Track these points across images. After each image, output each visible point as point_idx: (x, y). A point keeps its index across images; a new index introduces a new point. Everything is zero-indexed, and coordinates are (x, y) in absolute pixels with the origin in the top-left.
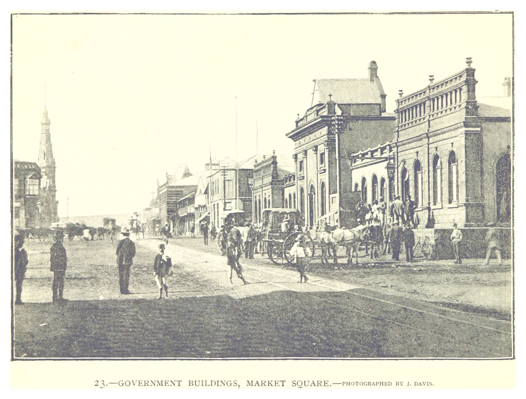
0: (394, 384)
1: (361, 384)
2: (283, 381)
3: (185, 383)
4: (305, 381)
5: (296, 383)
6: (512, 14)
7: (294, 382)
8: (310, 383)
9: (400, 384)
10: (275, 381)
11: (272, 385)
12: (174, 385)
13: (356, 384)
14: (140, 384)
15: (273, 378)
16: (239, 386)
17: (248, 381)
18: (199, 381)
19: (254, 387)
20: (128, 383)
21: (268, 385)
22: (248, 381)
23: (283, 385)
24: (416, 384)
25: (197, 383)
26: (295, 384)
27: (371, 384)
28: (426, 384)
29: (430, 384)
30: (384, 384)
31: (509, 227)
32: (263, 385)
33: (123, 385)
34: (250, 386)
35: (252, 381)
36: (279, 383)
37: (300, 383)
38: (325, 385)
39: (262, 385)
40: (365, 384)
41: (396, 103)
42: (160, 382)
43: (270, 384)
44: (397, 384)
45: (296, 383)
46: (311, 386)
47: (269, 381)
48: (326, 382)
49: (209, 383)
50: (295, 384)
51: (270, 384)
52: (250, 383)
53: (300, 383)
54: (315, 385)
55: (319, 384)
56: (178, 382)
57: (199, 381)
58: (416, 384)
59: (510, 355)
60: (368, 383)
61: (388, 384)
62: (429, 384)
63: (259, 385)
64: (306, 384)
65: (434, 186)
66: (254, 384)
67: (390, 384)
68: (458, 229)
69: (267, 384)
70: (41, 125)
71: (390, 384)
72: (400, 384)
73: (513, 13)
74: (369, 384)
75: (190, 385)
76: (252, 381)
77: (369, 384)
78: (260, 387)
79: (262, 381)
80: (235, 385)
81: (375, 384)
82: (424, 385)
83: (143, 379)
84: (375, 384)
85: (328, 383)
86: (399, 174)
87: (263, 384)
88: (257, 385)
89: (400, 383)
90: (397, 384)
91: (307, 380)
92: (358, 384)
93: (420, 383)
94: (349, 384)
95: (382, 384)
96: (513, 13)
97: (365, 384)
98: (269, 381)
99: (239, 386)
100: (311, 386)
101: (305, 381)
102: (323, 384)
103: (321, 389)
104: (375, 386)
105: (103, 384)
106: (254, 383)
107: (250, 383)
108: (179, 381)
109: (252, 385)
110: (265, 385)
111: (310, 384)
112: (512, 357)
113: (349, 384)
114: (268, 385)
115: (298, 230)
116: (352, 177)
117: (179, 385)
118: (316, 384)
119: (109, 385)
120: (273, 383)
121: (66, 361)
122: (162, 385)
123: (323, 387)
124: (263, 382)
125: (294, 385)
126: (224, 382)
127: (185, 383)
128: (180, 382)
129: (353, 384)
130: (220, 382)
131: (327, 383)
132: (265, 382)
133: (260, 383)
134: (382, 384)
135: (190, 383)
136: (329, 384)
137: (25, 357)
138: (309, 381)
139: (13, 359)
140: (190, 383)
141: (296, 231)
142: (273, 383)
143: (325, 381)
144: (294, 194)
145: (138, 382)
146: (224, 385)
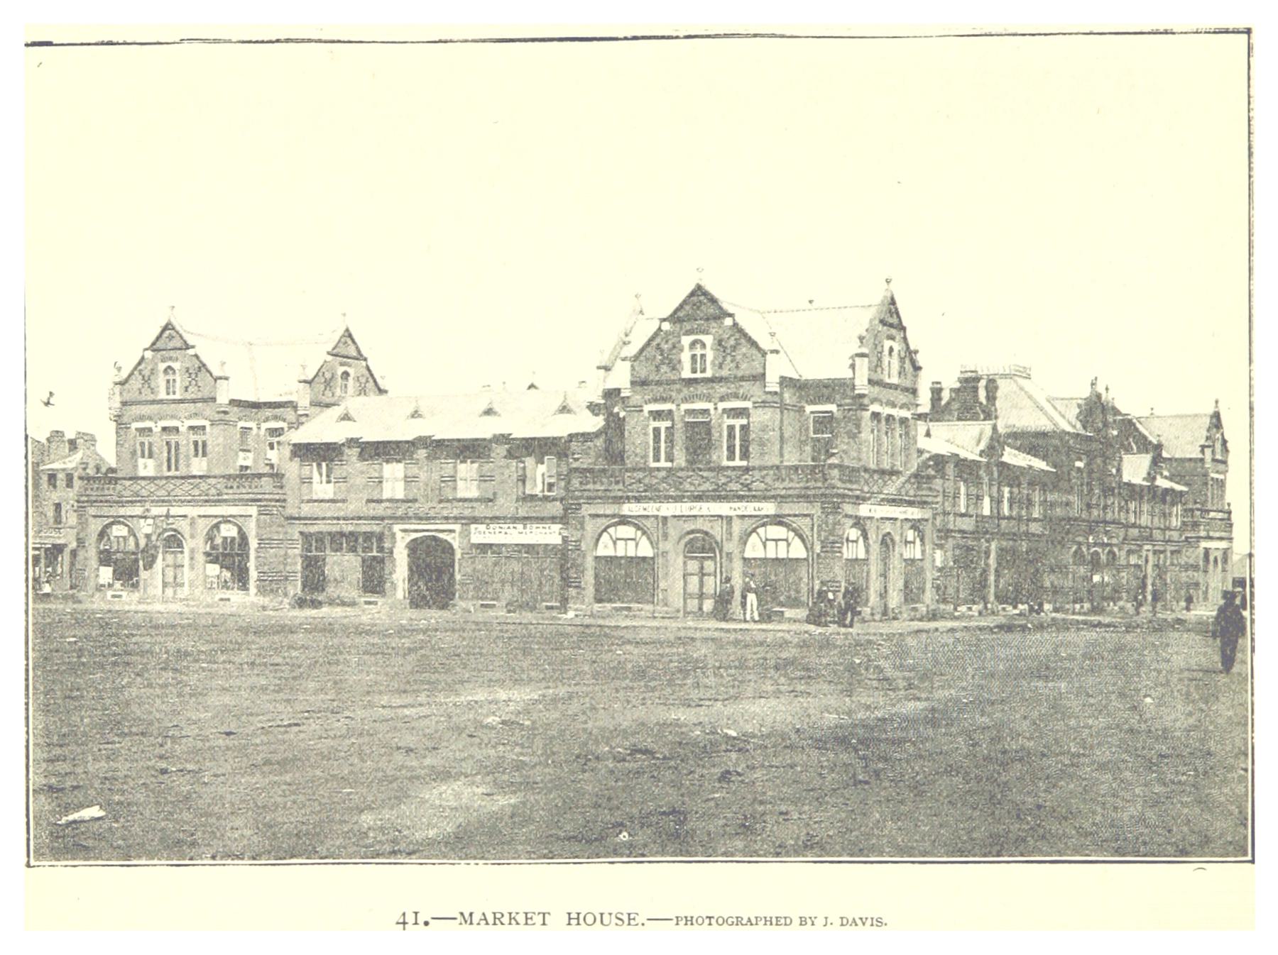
0: (796, 921)
1: (720, 921)
2: (544, 914)
3: (557, 919)
4: (602, 914)
6: (1246, 36)
9: (809, 922)
10: (526, 914)
11: (518, 924)
13: (707, 921)
15: (519, 906)
18: (610, 914)
19: (475, 926)
20: (590, 919)
23: (544, 924)
24: (844, 922)
27: (744, 922)
28: (869, 922)
29: (879, 922)
30: (774, 921)
31: (316, 549)
32: (497, 922)
34: (467, 926)
35: (471, 914)
36: (535, 917)
40: (730, 922)
42: (467, 916)
43: (513, 921)
44: (803, 922)
47: (510, 914)
51: (513, 921)
57: (610, 914)
58: (844, 922)
59: (1245, 854)
60: (735, 920)
62: (875, 922)
63: (487, 924)
65: (440, 444)
66: (475, 920)
69: (506, 920)
72: (809, 922)
73: (1248, 31)
75: (569, 924)
76: (471, 914)
78: (491, 927)
79: (494, 914)
81: (754, 921)
82: (864, 924)
83: (520, 907)
85: (637, 917)
87: (497, 919)
91: (869, 917)
92: (713, 921)
93: (749, 920)
94: (689, 921)
95: (768, 921)
96: (1248, 31)
97: (730, 922)
98: (510, 914)
101: (602, 914)
106: (476, 919)
109: (471, 923)
112: (1249, 858)
113: (689, 921)
118: (490, 919)
119: (432, 922)
133: (490, 919)
134: (768, 921)
135: (570, 919)
136: (639, 920)
139: (1253, 862)
140: (574, 919)
142: (521, 918)
144: (196, 455)
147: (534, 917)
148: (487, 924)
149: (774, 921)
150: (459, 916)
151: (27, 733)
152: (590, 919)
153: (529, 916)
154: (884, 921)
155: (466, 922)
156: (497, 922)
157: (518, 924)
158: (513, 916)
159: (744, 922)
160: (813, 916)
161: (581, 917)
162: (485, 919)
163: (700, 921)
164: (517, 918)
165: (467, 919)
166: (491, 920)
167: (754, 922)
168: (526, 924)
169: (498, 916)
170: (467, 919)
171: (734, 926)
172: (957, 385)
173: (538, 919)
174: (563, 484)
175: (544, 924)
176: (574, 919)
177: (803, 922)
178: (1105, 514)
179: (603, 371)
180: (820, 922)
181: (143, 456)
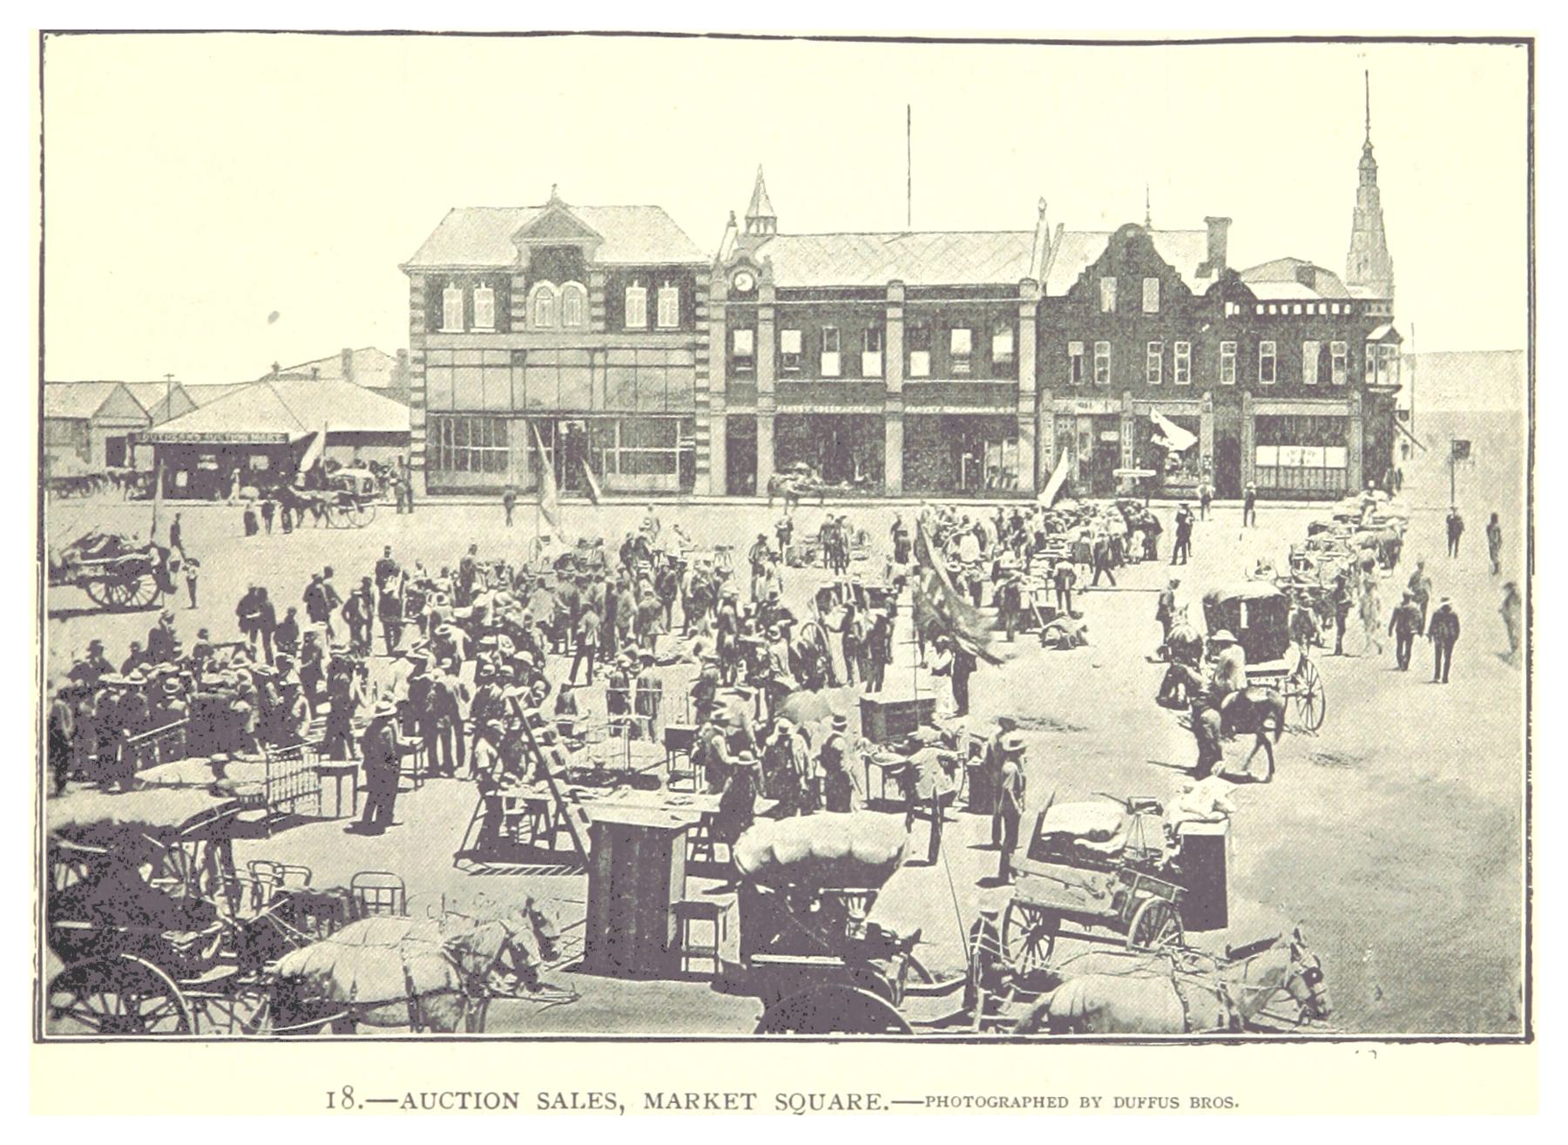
0: (1075, 1102)
1: (981, 1102)
2: (748, 1096)
4: (812, 1096)
5: (787, 1100)
7: (781, 1098)
8: (828, 1100)
9: (1092, 1102)
10: (727, 1096)
11: (716, 1107)
12: (515, 1104)
13: (964, 1102)
16: (622, 1108)
17: (648, 1095)
18: (434, 1094)
19: (664, 1110)
20: (492, 1101)
22: (648, 1095)
23: (463, 1107)
24: (1195, 1103)
25: (1131, 1102)
26: (783, 1102)
27: (1009, 1103)
29: (1228, 1103)
30: (1046, 1102)
32: (853, 1105)
34: (655, 1110)
35: (660, 1095)
37: (797, 1102)
38: (869, 1108)
39: (688, 1107)
40: (992, 1103)
41: (405, 282)
42: (654, 1097)
43: (710, 1105)
45: (787, 1100)
46: (668, 1107)
47: (707, 1095)
49: (583, 1099)
50: (783, 1102)
51: (710, 1105)
52: (654, 1101)
53: (797, 1102)
55: (853, 1104)
56: (460, 1096)
57: (434, 1094)
58: (1195, 1103)
61: (1057, 1102)
63: (679, 1107)
64: (817, 1104)
66: (665, 1103)
67: (1063, 1102)
68: (937, 729)
69: (701, 1102)
70: (408, 306)
71: (1063, 1102)
72: (1092, 1102)
74: (1003, 1102)
76: (660, 1095)
77: (1003, 1102)
78: (846, 1111)
79: (688, 1095)
80: (611, 1105)
81: (1021, 1102)
84: (1021, 1102)
87: (691, 1102)
88: (675, 1105)
89: (1091, 1102)
90: (1084, 1102)
91: (817, 1092)
92: (972, 1102)
94: (943, 1102)
95: (1039, 1102)
97: (992, 1103)
98: (707, 1095)
99: (622, 1108)
100: (668, 1107)
101: (812, 1096)
102: (864, 1103)
103: (861, 1116)
104: (1022, 1109)
106: (665, 1100)
107: (654, 1101)
108: (748, 1096)
109: (660, 1107)
110: (696, 1107)
113: (943, 1102)
117: (748, 1107)
118: (683, 1101)
119: (367, 1105)
120: (720, 1101)
121: (1062, 1046)
122: (660, 1107)
125: (781, 1106)
127: (764, 1102)
128: (752, 1097)
129: (956, 1102)
131: (875, 1102)
132: (698, 1097)
134: (1039, 1102)
136: (881, 1102)
138: (822, 1096)
142: (720, 1101)
143: (869, 1096)
147: (737, 1099)
148: (679, 1107)
149: (1046, 1102)
152: (492, 1101)
153: (730, 1098)
154: (1234, 1102)
155: (653, 1105)
160: (1097, 1096)
161: (482, 1098)
162: (677, 1102)
163: (956, 1102)
164: (716, 1100)
168: (591, 1107)
169: (854, 1098)
171: (998, 1108)
172: (88, 653)
173: (741, 1102)
174: (248, 647)
177: (1084, 1102)
178: (407, 776)
180: (1185, 1102)
181: (613, 470)
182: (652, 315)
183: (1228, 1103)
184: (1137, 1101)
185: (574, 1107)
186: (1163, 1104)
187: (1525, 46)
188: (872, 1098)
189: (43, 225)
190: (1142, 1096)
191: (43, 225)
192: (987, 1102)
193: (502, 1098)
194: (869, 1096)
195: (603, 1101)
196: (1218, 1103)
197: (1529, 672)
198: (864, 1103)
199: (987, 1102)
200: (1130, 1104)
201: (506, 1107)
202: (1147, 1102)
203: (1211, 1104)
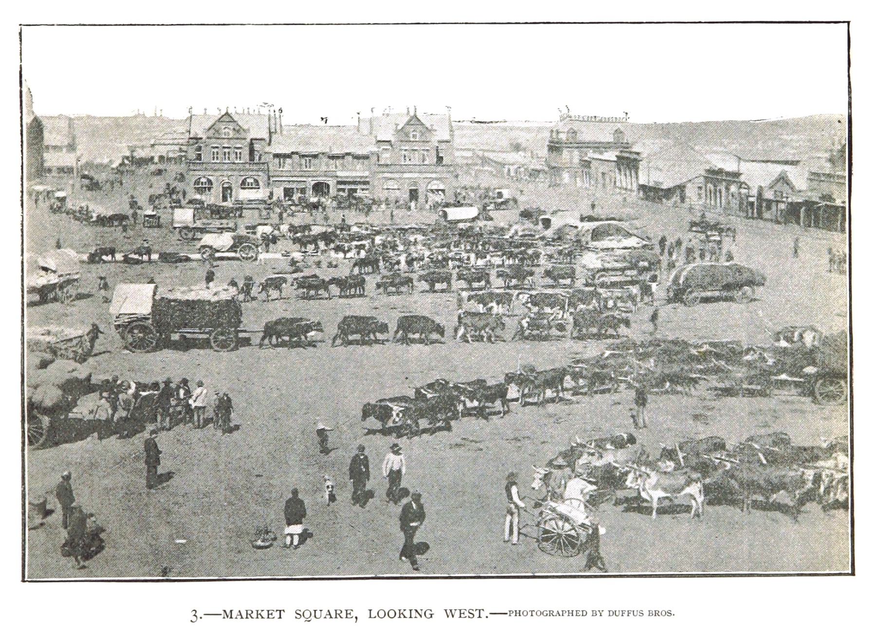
0: (590, 613)
1: (539, 613)
2: (280, 611)
3: (290, 615)
4: (315, 611)
5: (302, 614)
7: (298, 612)
8: (324, 613)
9: (598, 614)
10: (268, 611)
12: (453, 616)
13: (530, 614)
14: (462, 615)
16: (356, 618)
17: (225, 611)
20: (392, 614)
21: (257, 618)
22: (225, 611)
23: (480, 617)
26: (299, 614)
29: (669, 613)
30: (575, 613)
32: (249, 616)
33: (431, 617)
35: (231, 611)
37: (307, 614)
39: (247, 618)
40: (545, 614)
42: (228, 612)
43: (259, 616)
44: (594, 613)
45: (302, 614)
47: (257, 611)
48: (348, 612)
50: (299, 614)
51: (259, 616)
54: (331, 617)
55: (338, 615)
61: (581, 613)
63: (242, 618)
67: (584, 614)
69: (254, 615)
73: (848, 23)
74: (551, 613)
76: (231, 611)
77: (551, 613)
78: (334, 620)
79: (336, 611)
86: (723, 198)
87: (249, 615)
91: (318, 609)
92: (534, 613)
94: (518, 613)
95: (571, 613)
96: (848, 23)
97: (545, 614)
98: (257, 611)
99: (356, 618)
101: (315, 611)
102: (344, 615)
104: (561, 617)
105: (195, 615)
109: (231, 618)
111: (324, 615)
113: (518, 613)
114: (257, 618)
115: (285, 280)
116: (773, 118)
119: (204, 617)
120: (265, 614)
122: (231, 618)
123: (344, 619)
124: (249, 612)
125: (298, 616)
126: (420, 612)
127: (290, 615)
129: (525, 613)
130: (413, 612)
134: (571, 613)
137: (846, 382)
141: (290, 280)
142: (265, 614)
143: (347, 611)
145: (458, 612)
146: (421, 616)
149: (575, 613)
150: (222, 613)
151: (22, 192)
153: (462, 612)
156: (338, 616)
157: (262, 618)
158: (401, 612)
159: (554, 614)
160: (601, 610)
161: (398, 615)
163: (525, 613)
165: (229, 615)
166: (333, 615)
167: (561, 614)
170: (229, 615)
173: (277, 614)
175: (280, 618)
176: (449, 613)
177: (594, 613)
179: (406, 112)
180: (646, 613)
182: (753, 213)
183: (669, 613)
184: (621, 612)
185: (411, 617)
186: (635, 614)
187: (846, 24)
188: (270, 612)
189: (466, 23)
190: (260, 609)
191: (466, 23)
192: (542, 613)
193: (423, 615)
194: (347, 611)
195: (467, 614)
196: (664, 613)
197: (23, 285)
198: (254, 615)
199: (542, 613)
200: (617, 614)
201: (400, 617)
202: (626, 613)
203: (660, 614)
